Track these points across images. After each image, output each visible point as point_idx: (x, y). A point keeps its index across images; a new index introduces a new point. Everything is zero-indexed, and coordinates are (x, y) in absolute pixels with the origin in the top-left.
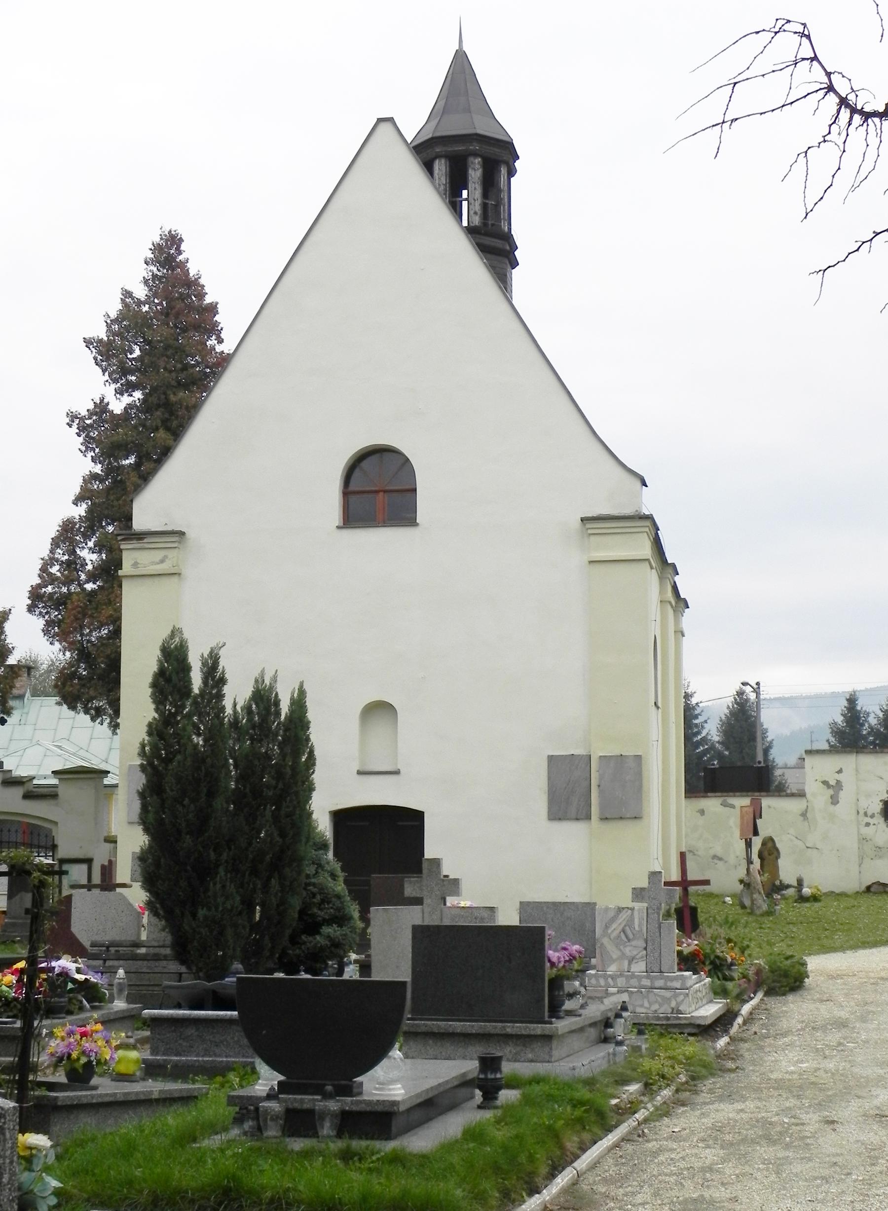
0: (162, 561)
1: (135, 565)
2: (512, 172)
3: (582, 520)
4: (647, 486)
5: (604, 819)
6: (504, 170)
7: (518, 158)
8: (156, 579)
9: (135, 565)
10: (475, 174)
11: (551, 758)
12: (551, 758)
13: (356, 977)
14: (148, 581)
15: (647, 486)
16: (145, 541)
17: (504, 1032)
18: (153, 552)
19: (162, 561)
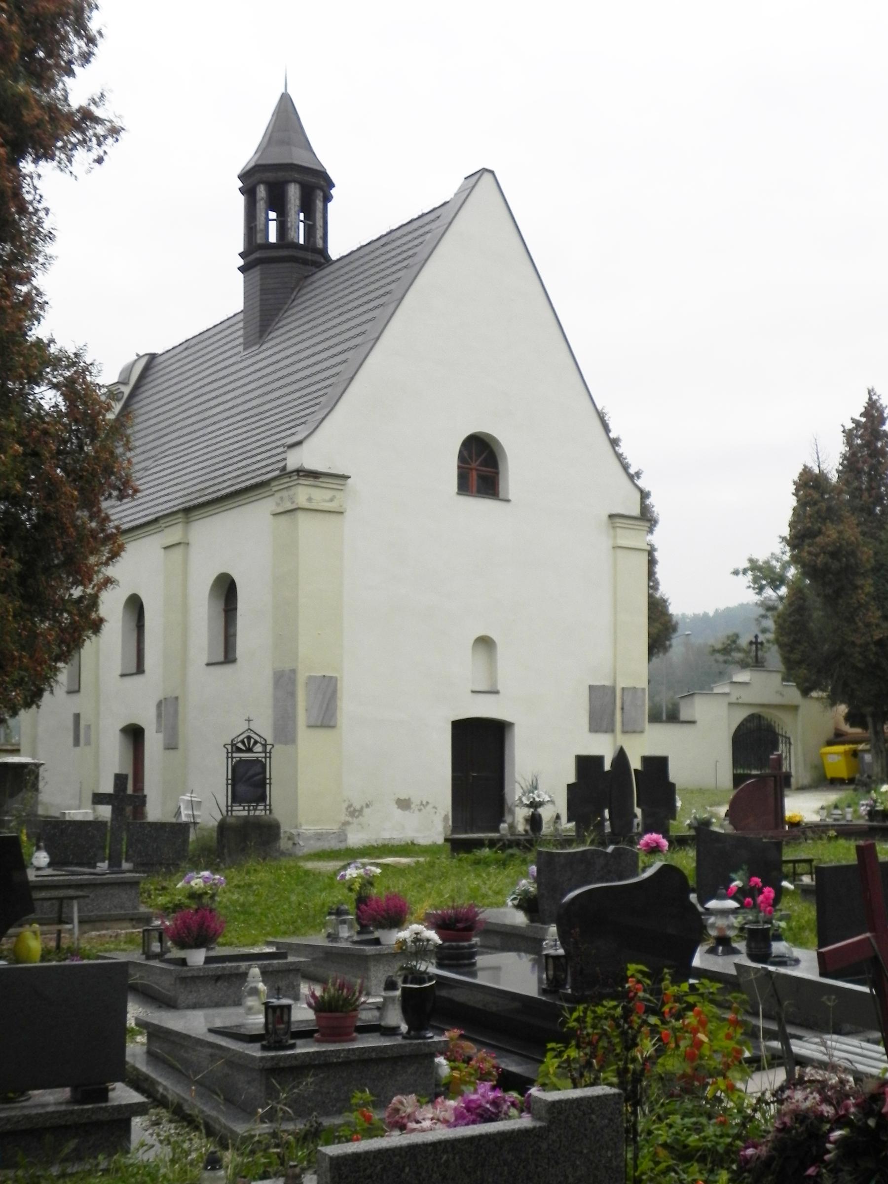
0: (331, 500)
1: (310, 500)
2: (327, 198)
3: (611, 516)
4: (349, 477)
5: (624, 732)
6: (320, 194)
7: (334, 186)
8: (327, 515)
9: (310, 500)
10: (293, 192)
11: (591, 688)
12: (591, 688)
13: (692, 853)
14: (320, 516)
15: (349, 477)
16: (321, 480)
17: (342, 846)
18: (324, 491)
19: (331, 500)
